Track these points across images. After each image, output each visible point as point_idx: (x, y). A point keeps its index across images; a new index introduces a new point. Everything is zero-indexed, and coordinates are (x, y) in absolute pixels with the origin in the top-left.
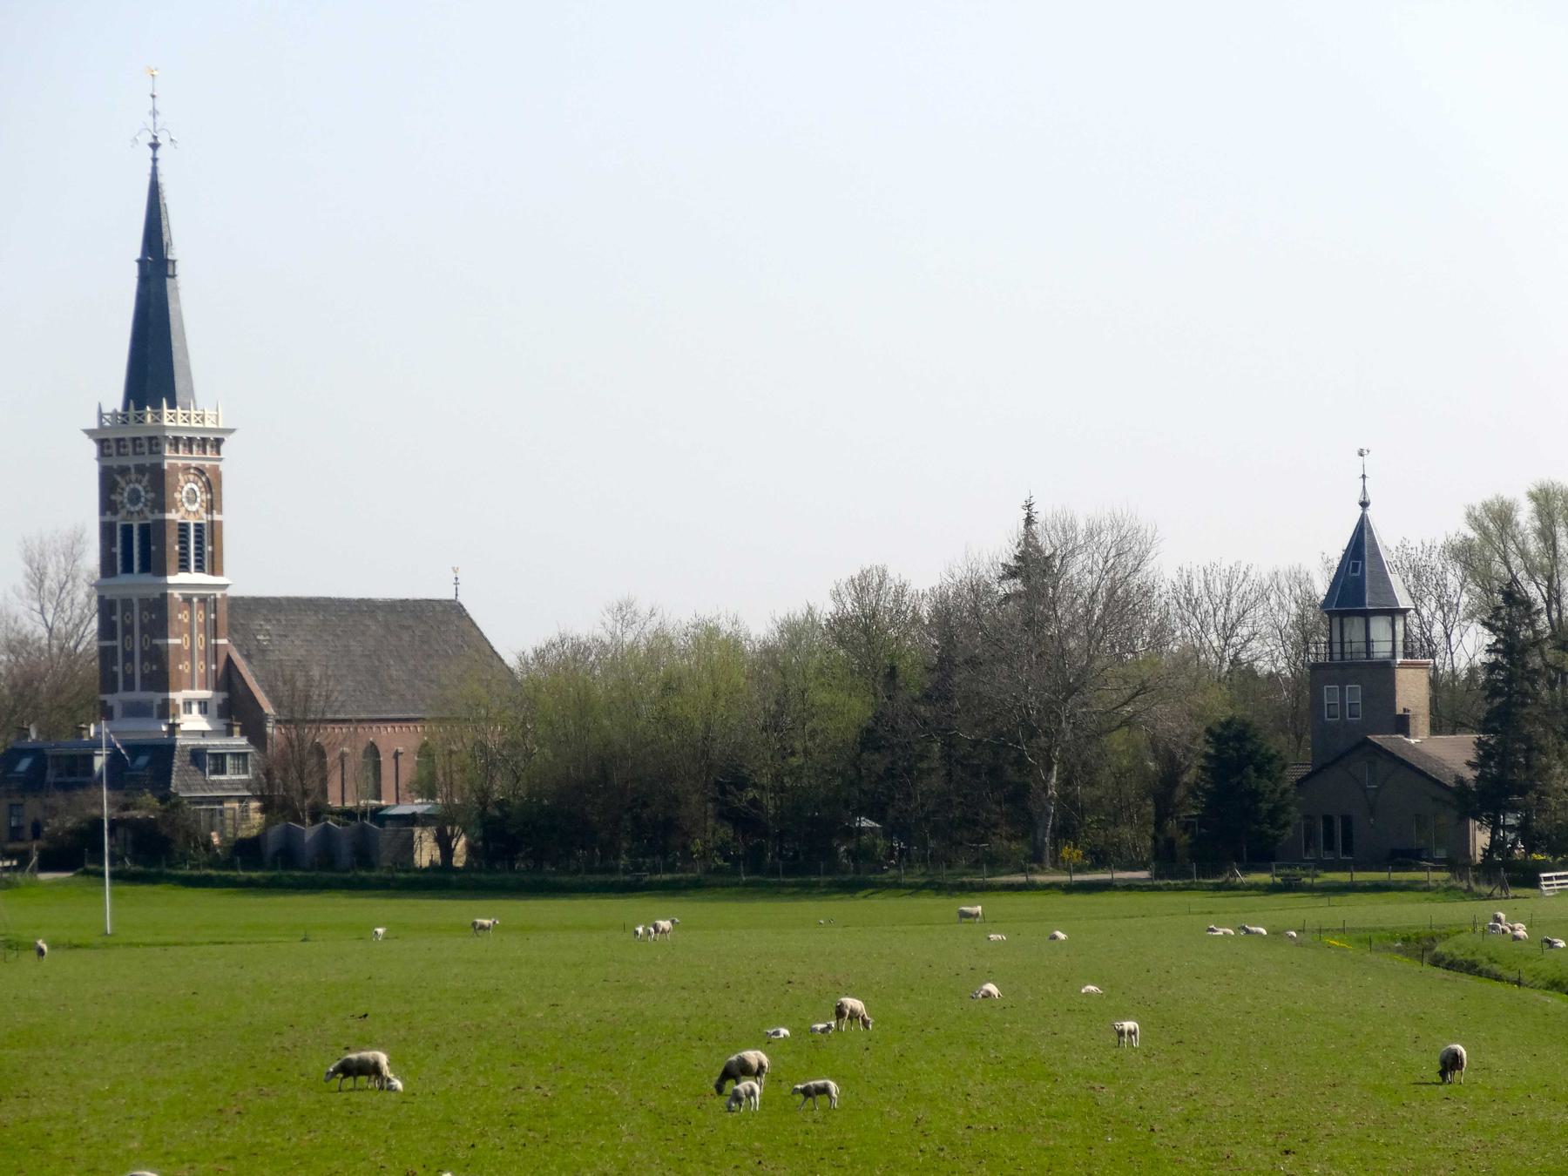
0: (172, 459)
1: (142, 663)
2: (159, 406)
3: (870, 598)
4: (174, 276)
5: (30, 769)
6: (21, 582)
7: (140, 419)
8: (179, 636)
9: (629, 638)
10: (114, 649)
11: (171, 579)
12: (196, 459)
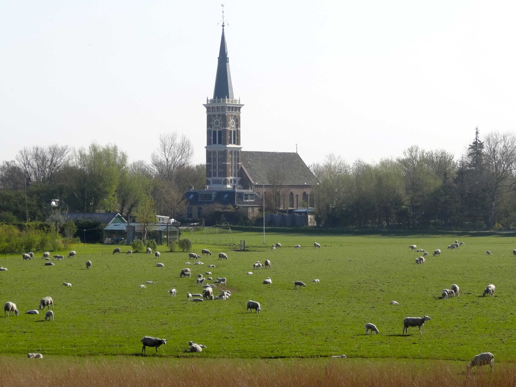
0: (228, 113)
3: (414, 154)
6: (159, 147)
9: (333, 164)
11: (228, 146)
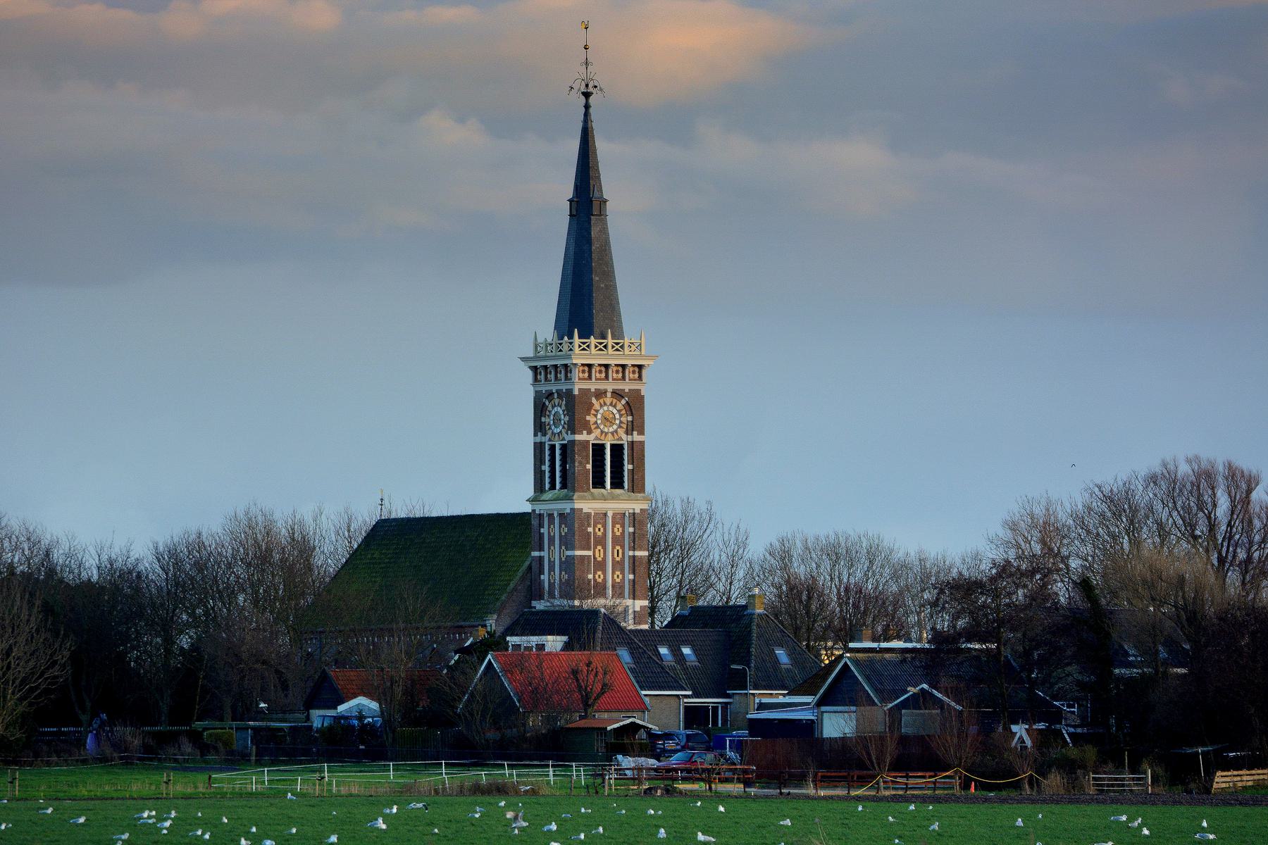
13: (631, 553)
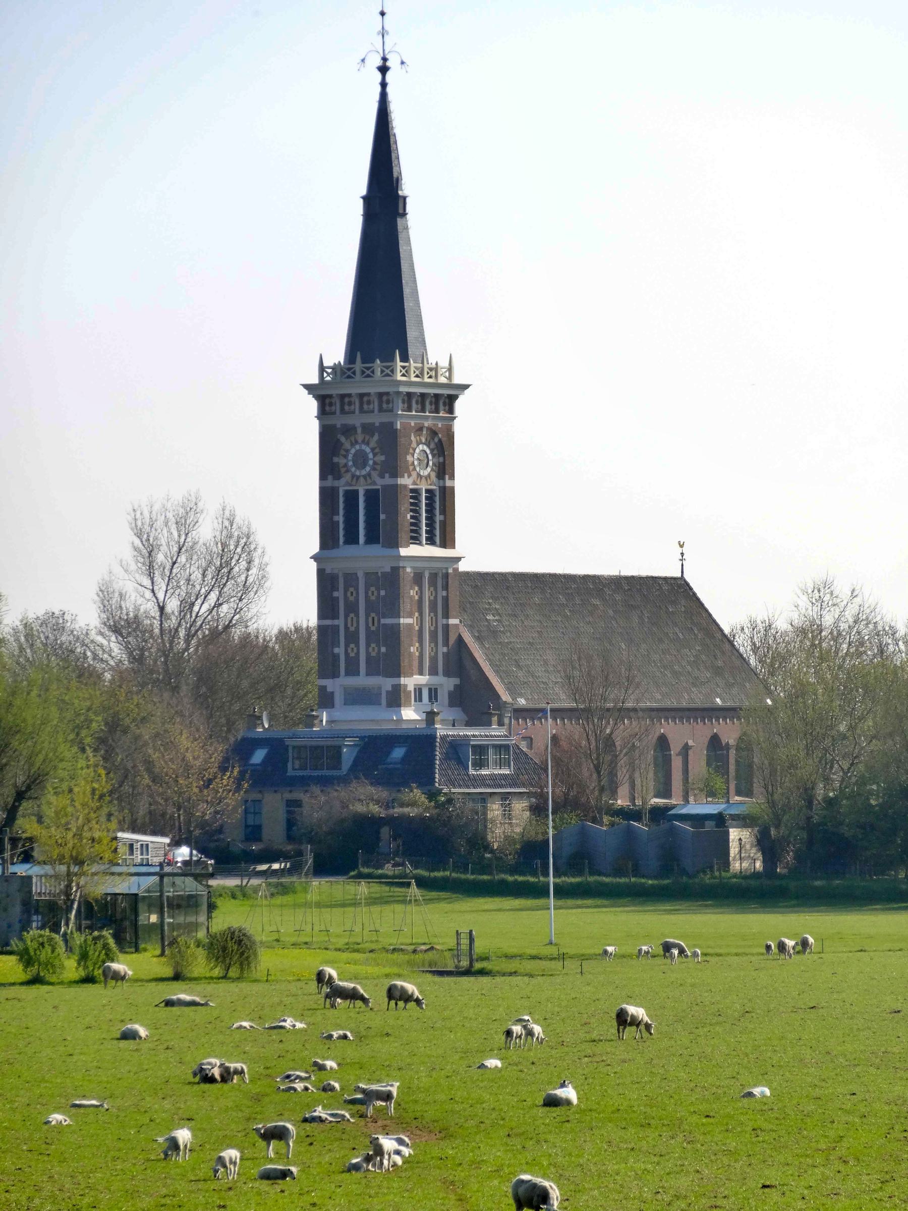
0: (405, 419)
1: (368, 645)
2: (392, 359)
4: (404, 214)
5: (265, 761)
6: (128, 555)
7: (368, 374)
8: (410, 616)
9: (828, 620)
10: (336, 629)
11: (403, 552)
12: (429, 420)
13: (445, 621)
